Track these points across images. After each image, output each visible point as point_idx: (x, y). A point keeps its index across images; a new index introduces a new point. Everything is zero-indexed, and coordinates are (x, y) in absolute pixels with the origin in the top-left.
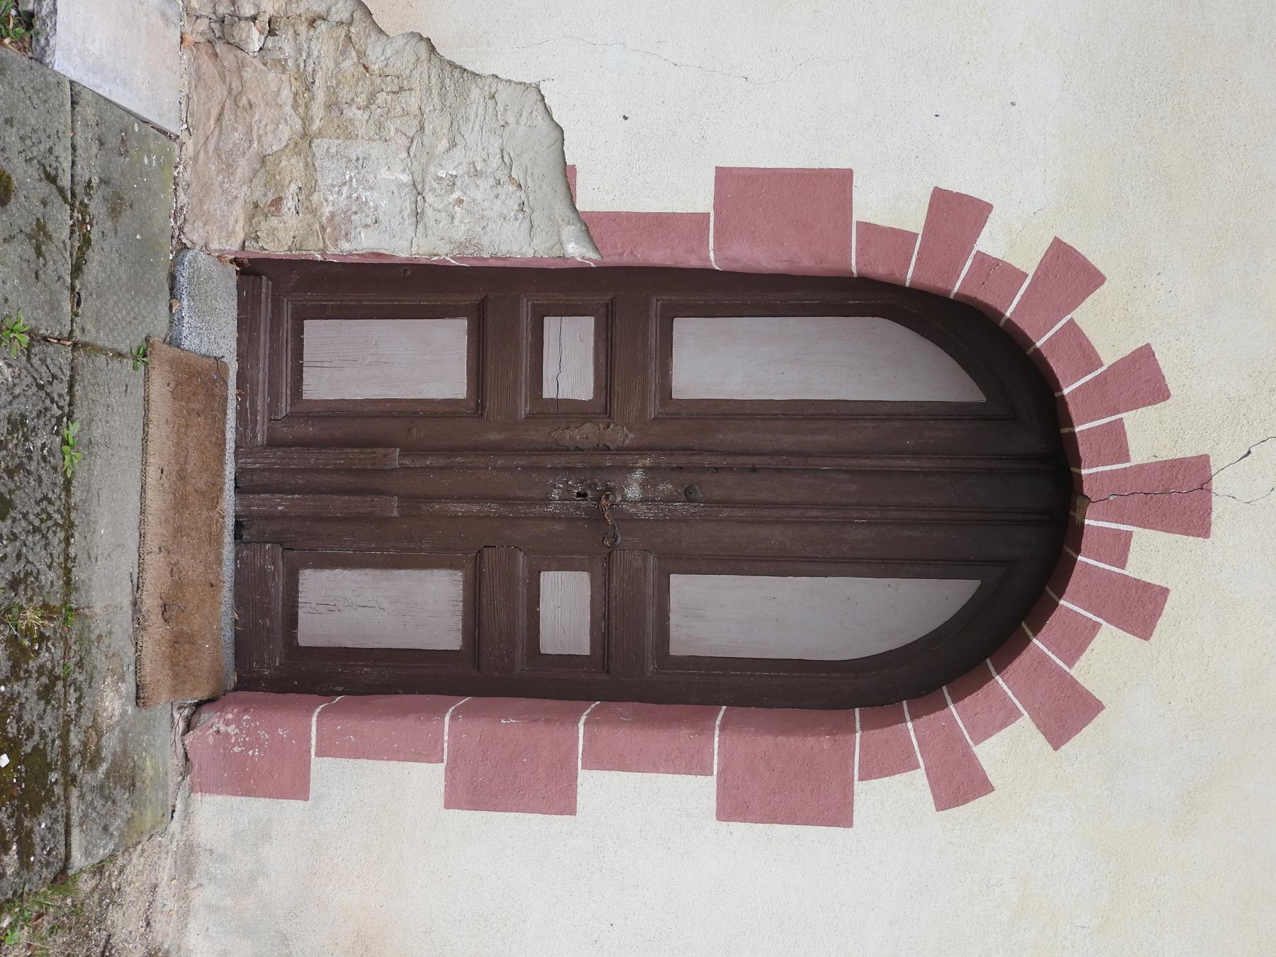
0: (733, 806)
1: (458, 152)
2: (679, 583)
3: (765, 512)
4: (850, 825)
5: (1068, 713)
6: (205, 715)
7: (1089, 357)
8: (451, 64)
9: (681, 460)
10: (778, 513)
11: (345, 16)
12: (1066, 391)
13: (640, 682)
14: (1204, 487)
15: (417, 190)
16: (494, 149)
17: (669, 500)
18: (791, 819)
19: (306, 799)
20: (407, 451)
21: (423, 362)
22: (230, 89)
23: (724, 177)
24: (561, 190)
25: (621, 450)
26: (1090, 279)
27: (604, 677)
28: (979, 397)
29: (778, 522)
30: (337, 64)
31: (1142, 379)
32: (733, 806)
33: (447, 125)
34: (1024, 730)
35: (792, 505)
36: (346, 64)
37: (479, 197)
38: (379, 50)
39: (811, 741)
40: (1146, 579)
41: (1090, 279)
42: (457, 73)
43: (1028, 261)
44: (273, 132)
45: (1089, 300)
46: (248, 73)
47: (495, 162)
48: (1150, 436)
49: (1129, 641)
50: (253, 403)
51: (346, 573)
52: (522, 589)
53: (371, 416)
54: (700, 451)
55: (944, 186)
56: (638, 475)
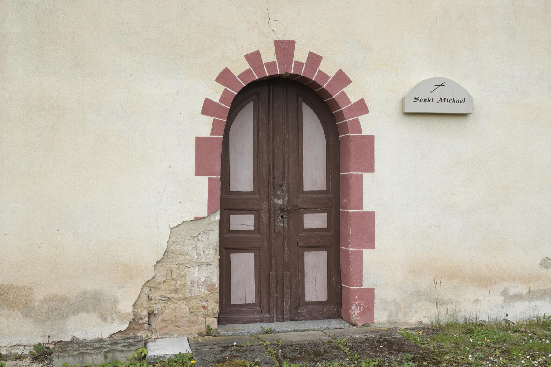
0: (371, 168)
1: (190, 252)
2: (306, 188)
3: (286, 163)
4: (374, 136)
5: (342, 79)
6: (353, 320)
7: (248, 72)
8: (164, 255)
9: (272, 187)
10: (286, 160)
11: (148, 289)
12: (257, 78)
13: (337, 196)
14: (282, 42)
15: (200, 265)
16: (189, 242)
17: (283, 191)
18: (373, 152)
19: (374, 289)
20: (271, 270)
21: (244, 264)
22: (170, 324)
23: (197, 174)
24: (201, 221)
25: (269, 206)
26: (226, 71)
27: (333, 209)
28: (252, 103)
29: (288, 158)
30: (163, 290)
31: (254, 58)
32: (371, 168)
33: (181, 256)
34: (347, 90)
35: (283, 156)
36: (163, 288)
37: (202, 246)
38: (159, 278)
39: (352, 147)
40: (307, 57)
41: (226, 71)
42: (166, 254)
43: (222, 88)
44: (183, 309)
45: (232, 72)
46: (166, 318)
47: (192, 241)
48: (269, 56)
49: (323, 62)
50: (258, 318)
51: (306, 287)
52: (309, 234)
53: (260, 282)
54: (269, 182)
55: (201, 111)
56: (276, 201)
